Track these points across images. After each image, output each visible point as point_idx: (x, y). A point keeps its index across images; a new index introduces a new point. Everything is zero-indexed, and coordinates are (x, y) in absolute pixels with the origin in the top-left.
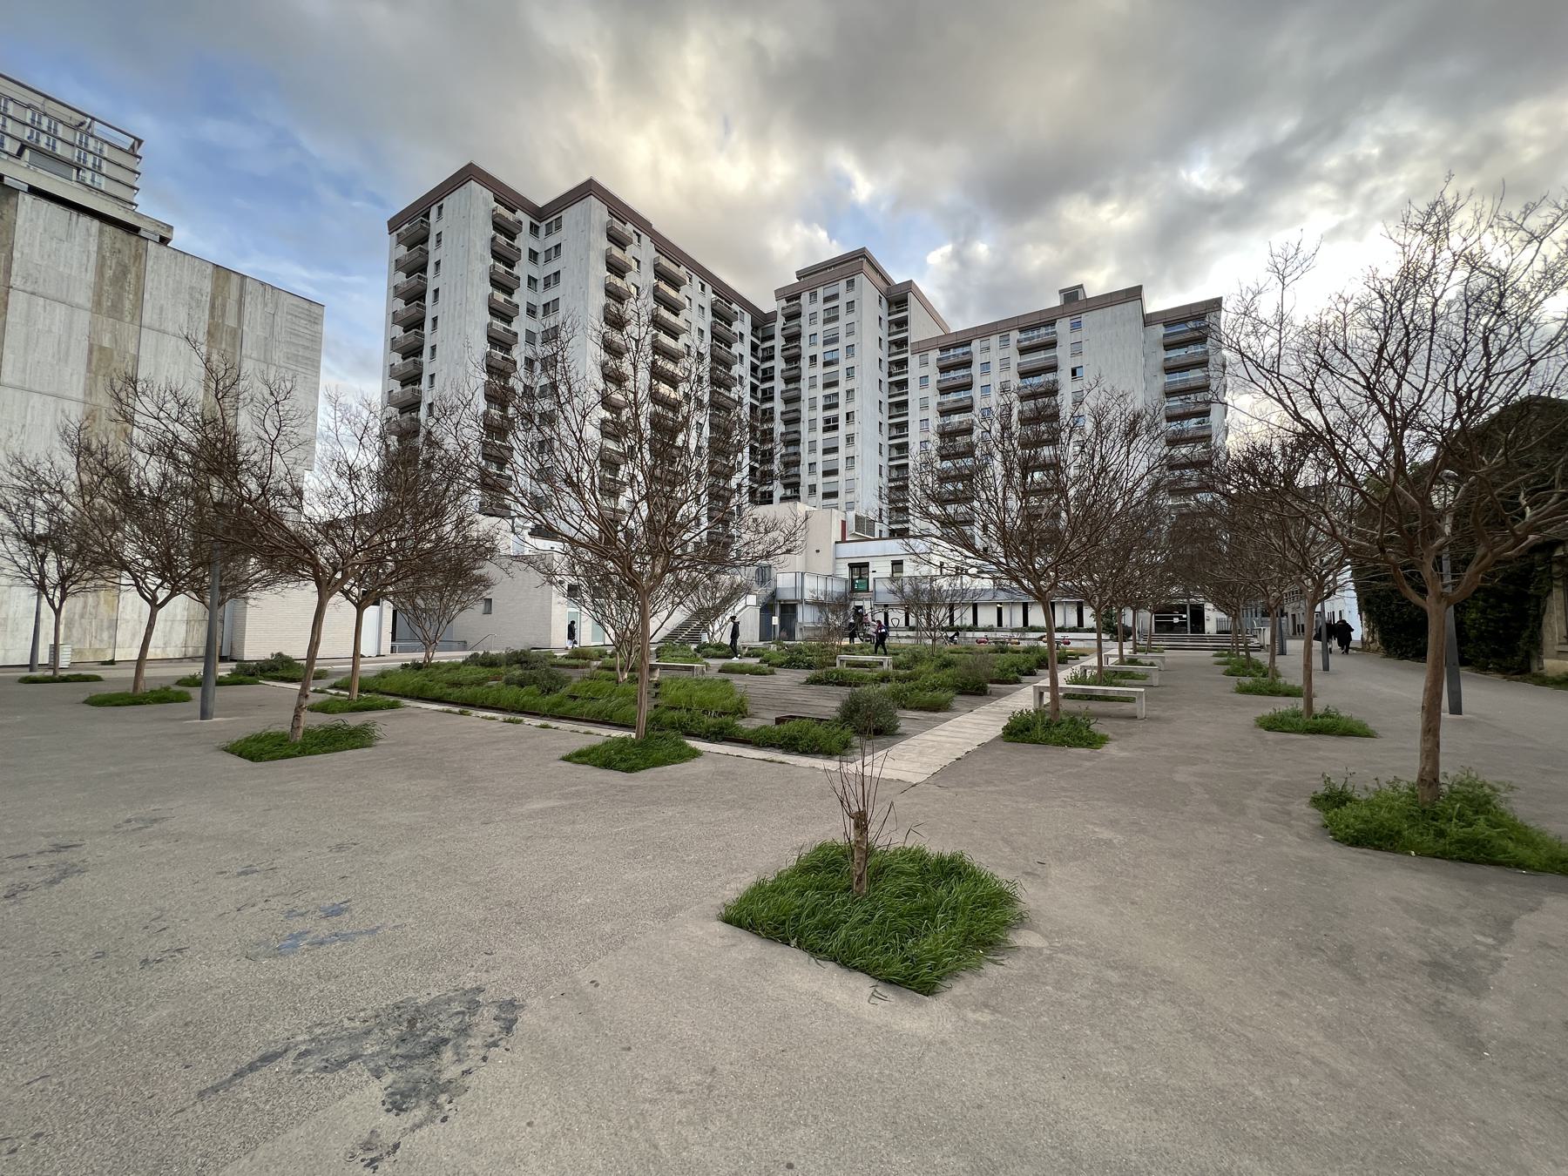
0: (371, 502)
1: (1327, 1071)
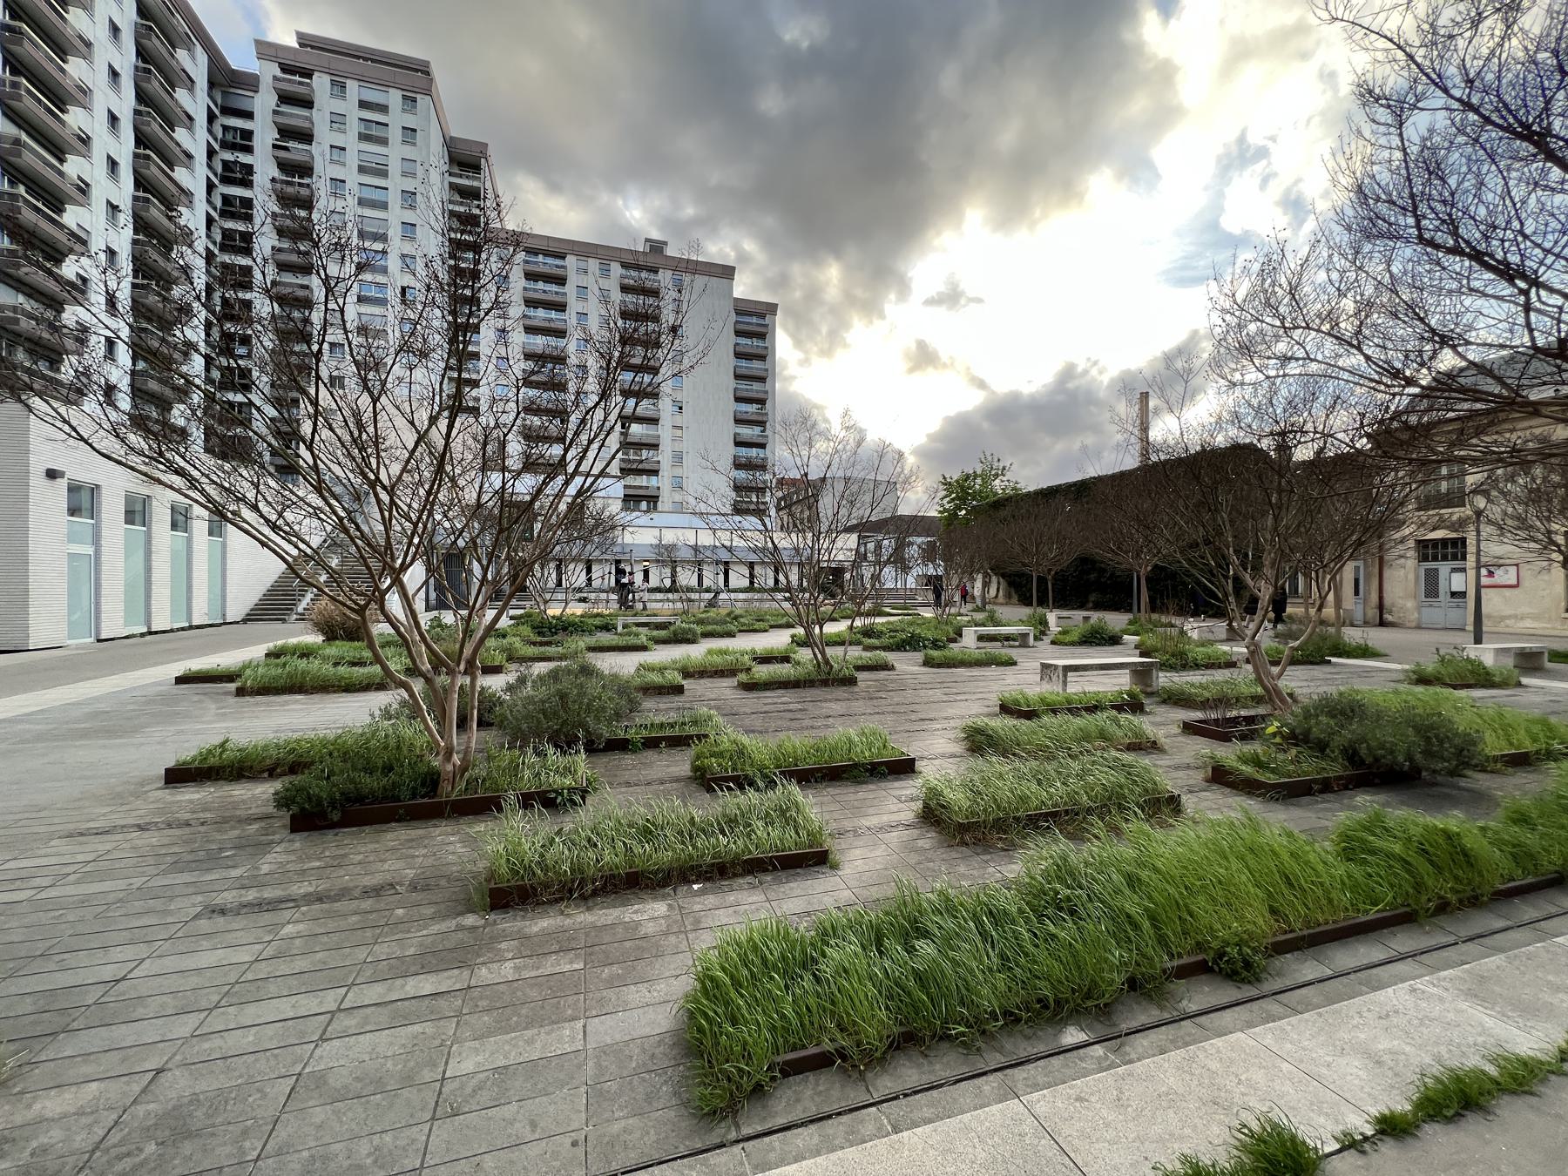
0: (606, 672)
1: (1485, 898)
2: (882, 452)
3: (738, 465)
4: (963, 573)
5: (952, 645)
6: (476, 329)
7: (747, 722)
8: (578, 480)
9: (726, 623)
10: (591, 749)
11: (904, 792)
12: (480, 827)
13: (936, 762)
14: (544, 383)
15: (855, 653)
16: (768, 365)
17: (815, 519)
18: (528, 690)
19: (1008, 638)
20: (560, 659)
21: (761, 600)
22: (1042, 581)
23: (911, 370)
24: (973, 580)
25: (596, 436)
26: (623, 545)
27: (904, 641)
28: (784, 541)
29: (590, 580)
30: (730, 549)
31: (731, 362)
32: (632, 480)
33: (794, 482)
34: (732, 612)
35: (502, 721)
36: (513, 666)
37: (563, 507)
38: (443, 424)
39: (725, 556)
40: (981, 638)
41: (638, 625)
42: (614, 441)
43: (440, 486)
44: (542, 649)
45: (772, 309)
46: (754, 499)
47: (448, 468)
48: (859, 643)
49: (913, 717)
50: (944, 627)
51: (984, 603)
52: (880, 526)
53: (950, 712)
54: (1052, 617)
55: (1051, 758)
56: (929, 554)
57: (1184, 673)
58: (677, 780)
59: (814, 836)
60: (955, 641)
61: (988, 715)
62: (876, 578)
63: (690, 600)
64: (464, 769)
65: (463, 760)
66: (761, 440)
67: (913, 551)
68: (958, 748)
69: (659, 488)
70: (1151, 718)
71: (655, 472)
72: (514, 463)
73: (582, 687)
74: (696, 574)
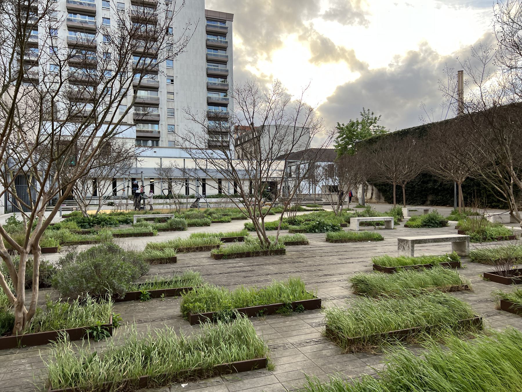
2: (300, 108)
3: (210, 118)
4: (350, 184)
5: (344, 229)
6: (35, 27)
7: (217, 279)
8: (104, 127)
9: (203, 217)
10: (117, 299)
11: (315, 321)
12: (40, 353)
13: (334, 301)
14: (79, 64)
15: (284, 234)
16: (228, 53)
17: (258, 151)
18: (74, 263)
19: (378, 224)
20: (96, 242)
21: (226, 203)
22: (399, 188)
23: (311, 61)
24: (357, 188)
25: (115, 98)
26: (137, 169)
27: (314, 226)
28: (240, 166)
29: (115, 191)
30: (205, 171)
31: (203, 51)
32: (142, 127)
33: (244, 128)
34: (207, 210)
35: (56, 284)
36: (64, 248)
37: (95, 144)
38: (12, 90)
39: (202, 175)
40: (362, 224)
41: (147, 220)
42: (128, 101)
43: (10, 130)
44: (84, 236)
45: (230, 17)
46: (220, 139)
47: (16, 119)
48: (286, 228)
49: (320, 273)
50: (338, 218)
51: (364, 202)
52: (299, 156)
53: (343, 270)
54: (405, 210)
55: (404, 297)
56: (330, 172)
57: (484, 244)
58: (172, 318)
59: (258, 351)
60: (345, 226)
61: (366, 271)
62: (297, 186)
63: (181, 203)
64: (31, 316)
65: (30, 310)
66: (224, 102)
67: (320, 171)
68: (347, 292)
69: (159, 132)
70: (464, 271)
71: (157, 122)
72: (62, 115)
73: (109, 260)
74: (184, 187)
